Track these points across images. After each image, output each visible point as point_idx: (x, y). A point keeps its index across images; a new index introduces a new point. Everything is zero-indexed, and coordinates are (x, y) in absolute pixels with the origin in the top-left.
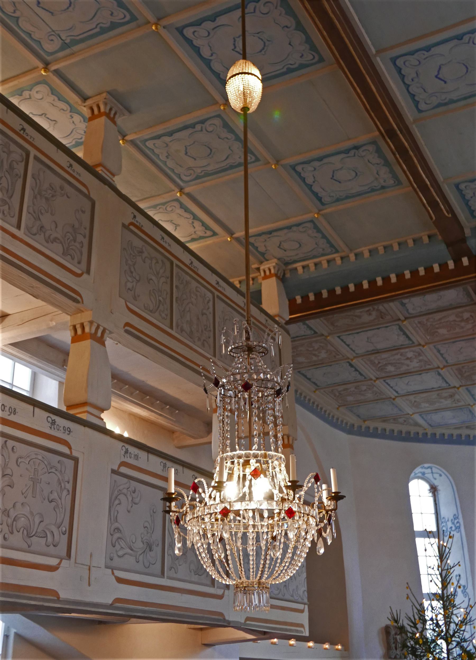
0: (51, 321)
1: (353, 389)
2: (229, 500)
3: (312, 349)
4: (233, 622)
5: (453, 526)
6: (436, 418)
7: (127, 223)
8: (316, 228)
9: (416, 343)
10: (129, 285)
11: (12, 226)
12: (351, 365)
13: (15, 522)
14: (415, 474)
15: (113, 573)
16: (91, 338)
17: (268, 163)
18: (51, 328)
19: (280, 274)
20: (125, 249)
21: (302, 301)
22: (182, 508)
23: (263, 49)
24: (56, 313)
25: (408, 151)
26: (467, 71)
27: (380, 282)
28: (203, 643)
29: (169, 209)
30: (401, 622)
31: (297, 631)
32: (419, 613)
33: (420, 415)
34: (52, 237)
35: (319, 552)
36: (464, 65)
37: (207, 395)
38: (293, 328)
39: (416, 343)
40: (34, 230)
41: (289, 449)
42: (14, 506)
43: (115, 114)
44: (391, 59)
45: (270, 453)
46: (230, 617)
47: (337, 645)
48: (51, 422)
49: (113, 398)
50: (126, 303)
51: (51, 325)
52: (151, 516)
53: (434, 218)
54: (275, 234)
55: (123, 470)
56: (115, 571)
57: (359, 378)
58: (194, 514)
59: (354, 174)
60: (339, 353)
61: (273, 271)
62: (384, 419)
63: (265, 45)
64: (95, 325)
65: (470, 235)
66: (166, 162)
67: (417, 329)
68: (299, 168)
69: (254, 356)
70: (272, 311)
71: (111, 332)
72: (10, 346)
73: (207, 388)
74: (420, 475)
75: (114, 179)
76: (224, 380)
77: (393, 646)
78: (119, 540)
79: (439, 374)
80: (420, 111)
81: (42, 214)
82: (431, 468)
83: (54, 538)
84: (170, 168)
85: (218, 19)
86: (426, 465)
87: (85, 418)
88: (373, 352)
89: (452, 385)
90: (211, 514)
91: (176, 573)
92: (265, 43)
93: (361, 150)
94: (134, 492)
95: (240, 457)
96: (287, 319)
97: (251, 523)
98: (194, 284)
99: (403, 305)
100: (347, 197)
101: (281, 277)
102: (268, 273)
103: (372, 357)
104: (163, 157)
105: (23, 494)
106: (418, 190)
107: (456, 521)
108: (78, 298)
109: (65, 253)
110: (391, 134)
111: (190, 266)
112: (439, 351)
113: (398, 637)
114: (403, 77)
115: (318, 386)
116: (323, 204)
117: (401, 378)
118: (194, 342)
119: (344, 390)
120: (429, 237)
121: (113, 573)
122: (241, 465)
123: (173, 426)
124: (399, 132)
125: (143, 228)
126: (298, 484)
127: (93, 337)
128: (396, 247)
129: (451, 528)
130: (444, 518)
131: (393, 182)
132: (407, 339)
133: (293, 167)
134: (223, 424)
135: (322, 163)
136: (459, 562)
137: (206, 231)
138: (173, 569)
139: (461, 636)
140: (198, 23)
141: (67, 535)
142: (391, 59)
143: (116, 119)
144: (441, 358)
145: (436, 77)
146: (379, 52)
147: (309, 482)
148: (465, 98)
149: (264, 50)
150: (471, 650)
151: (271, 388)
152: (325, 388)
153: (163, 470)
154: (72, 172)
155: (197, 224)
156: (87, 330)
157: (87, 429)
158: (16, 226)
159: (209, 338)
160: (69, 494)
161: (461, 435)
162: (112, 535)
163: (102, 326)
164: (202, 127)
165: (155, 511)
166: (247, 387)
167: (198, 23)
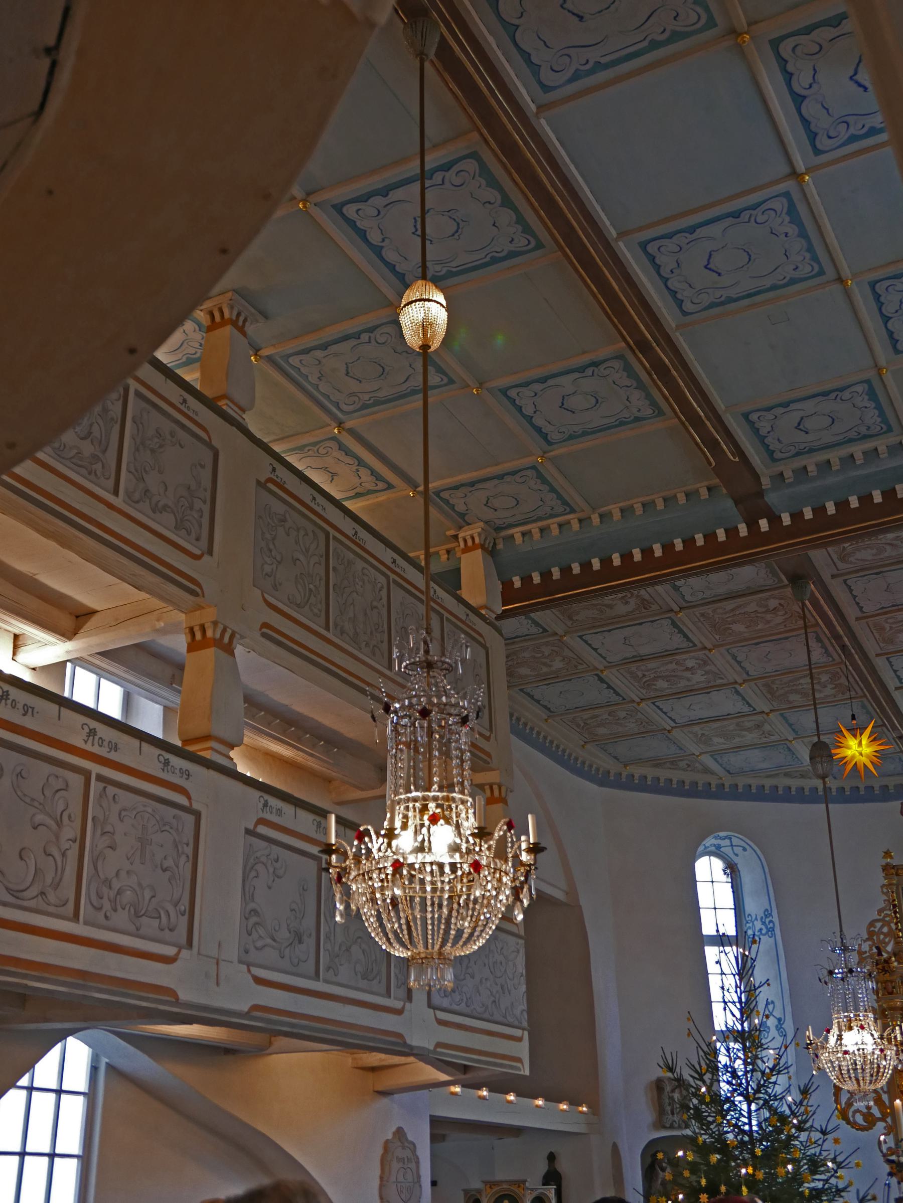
0: (158, 620)
1: (606, 716)
2: (401, 851)
3: (540, 655)
4: (417, 1047)
5: (763, 927)
6: (736, 760)
7: (263, 480)
8: (540, 476)
9: (699, 645)
10: (268, 569)
11: (107, 491)
12: (601, 680)
13: (118, 896)
14: (706, 848)
15: (249, 971)
16: (215, 646)
17: (468, 386)
18: (157, 631)
19: (489, 545)
20: (260, 517)
21: (522, 584)
22: (345, 862)
23: (457, 231)
24: (165, 610)
25: (670, 370)
26: (750, 259)
27: (637, 556)
28: (376, 1089)
29: (322, 451)
30: (678, 1070)
31: (512, 1067)
32: (707, 1058)
33: (712, 756)
34: (161, 504)
35: (516, 919)
36: (745, 251)
37: (374, 723)
38: (510, 625)
39: (699, 645)
40: (137, 496)
41: (501, 804)
42: (117, 874)
43: (245, 321)
44: (771, 42)
45: (454, 795)
46: (415, 1040)
47: (581, 1105)
48: (163, 761)
49: (246, 732)
50: (263, 597)
51: (158, 627)
52: (300, 895)
53: (714, 464)
54: (480, 486)
55: (262, 829)
56: (252, 969)
57: (616, 699)
58: (359, 869)
59: (593, 401)
60: (581, 662)
61: (477, 540)
62: (657, 763)
63: (458, 228)
64: (220, 628)
65: (769, 486)
66: (318, 385)
67: (700, 624)
68: (513, 393)
69: (435, 674)
70: (475, 600)
71: (242, 637)
72: (96, 655)
73: (376, 714)
74: (713, 849)
75: (244, 416)
76: (397, 705)
77: (668, 1108)
78: (257, 926)
79: (737, 692)
80: (685, 313)
81: (146, 471)
82: (731, 839)
83: (169, 919)
84: (324, 395)
85: (391, 193)
86: (722, 834)
87: (208, 757)
88: (633, 660)
89: (758, 710)
90: (380, 869)
91: (336, 975)
92: (458, 224)
93: (602, 367)
94: (277, 861)
95: (415, 800)
96: (499, 612)
97: (428, 878)
98: (360, 564)
99: (676, 588)
100: (585, 434)
101: (490, 549)
102: (470, 543)
103: (633, 667)
104: (313, 379)
105: (128, 859)
106: (687, 423)
107: (767, 920)
108: (198, 590)
109: (179, 526)
110: (643, 346)
111: (354, 538)
112: (735, 658)
113: (676, 1096)
114: (657, 268)
115: (551, 712)
116: (549, 443)
117: (679, 698)
118: (360, 649)
119: (592, 718)
120: (709, 489)
121: (249, 971)
122: (417, 810)
123: (329, 771)
124: (654, 344)
125: (285, 485)
126: (485, 831)
127: (217, 643)
128: (660, 505)
129: (761, 930)
130: (749, 915)
131: (652, 412)
132: (685, 639)
133: (504, 392)
134: (396, 760)
135: (545, 385)
136: (768, 980)
137: (377, 482)
138: (331, 969)
139: (770, 1091)
140: (364, 198)
141: (186, 917)
142: (771, 42)
143: (246, 329)
144: (738, 668)
145: (706, 267)
146: (621, 235)
147: (500, 830)
148: (750, 296)
149: (457, 234)
150: (784, 1111)
151: (456, 715)
152: (562, 715)
153: (316, 831)
154: (186, 410)
155: (364, 472)
156: (209, 633)
157: (212, 773)
158: (112, 492)
159: (382, 642)
160: (188, 861)
161: (777, 787)
162: (247, 919)
163: (230, 629)
164: (370, 337)
165: (305, 887)
166: (425, 713)
167: (364, 198)
